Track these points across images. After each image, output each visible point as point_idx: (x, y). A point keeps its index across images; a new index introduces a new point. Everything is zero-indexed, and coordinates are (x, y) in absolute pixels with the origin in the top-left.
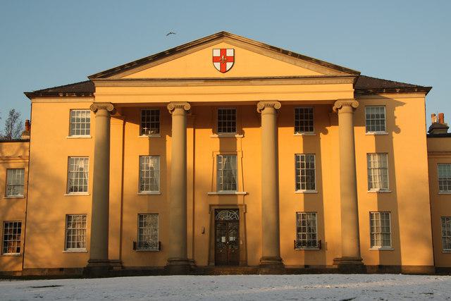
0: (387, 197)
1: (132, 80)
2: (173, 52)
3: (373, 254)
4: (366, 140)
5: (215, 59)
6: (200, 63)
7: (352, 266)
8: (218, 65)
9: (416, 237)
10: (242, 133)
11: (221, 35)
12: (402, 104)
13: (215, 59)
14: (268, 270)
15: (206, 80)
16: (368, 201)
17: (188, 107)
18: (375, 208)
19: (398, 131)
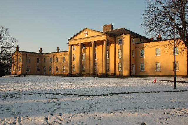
0: (121, 60)
1: (75, 39)
2: (77, 35)
3: (118, 73)
4: (118, 46)
5: (85, 34)
6: (82, 35)
7: (114, 76)
8: (85, 35)
9: (126, 69)
10: (97, 47)
11: (85, 29)
12: (125, 37)
13: (85, 34)
14: (133, 49)
15: (83, 38)
16: (118, 60)
17: (94, 42)
18: (119, 62)
19: (124, 44)
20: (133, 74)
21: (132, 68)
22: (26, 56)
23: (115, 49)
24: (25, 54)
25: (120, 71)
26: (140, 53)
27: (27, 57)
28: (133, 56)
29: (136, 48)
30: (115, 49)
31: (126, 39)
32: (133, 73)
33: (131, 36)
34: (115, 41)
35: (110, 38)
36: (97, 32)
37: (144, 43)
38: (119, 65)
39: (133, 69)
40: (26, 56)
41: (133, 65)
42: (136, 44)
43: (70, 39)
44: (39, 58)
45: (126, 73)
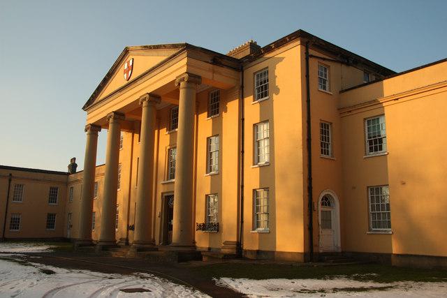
0: (267, 171)
1: (111, 95)
4: (252, 108)
12: (281, 59)
16: (252, 179)
18: (257, 186)
20: (331, 249)
21: (319, 217)
22: (10, 181)
23: (242, 120)
24: (7, 173)
25: (260, 233)
26: (361, 136)
27: (13, 183)
28: (324, 152)
29: (344, 111)
30: (242, 120)
31: (288, 68)
32: (330, 240)
33: (311, 52)
34: (242, 87)
35: (214, 72)
36: (306, 76)
37: (381, 80)
38: (258, 209)
39: (327, 223)
40: (10, 181)
41: (327, 201)
42: (342, 92)
43: (89, 105)
44: (55, 186)
45: (290, 241)
